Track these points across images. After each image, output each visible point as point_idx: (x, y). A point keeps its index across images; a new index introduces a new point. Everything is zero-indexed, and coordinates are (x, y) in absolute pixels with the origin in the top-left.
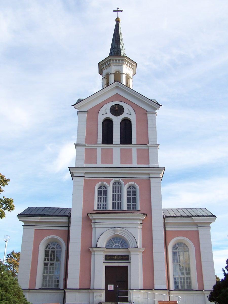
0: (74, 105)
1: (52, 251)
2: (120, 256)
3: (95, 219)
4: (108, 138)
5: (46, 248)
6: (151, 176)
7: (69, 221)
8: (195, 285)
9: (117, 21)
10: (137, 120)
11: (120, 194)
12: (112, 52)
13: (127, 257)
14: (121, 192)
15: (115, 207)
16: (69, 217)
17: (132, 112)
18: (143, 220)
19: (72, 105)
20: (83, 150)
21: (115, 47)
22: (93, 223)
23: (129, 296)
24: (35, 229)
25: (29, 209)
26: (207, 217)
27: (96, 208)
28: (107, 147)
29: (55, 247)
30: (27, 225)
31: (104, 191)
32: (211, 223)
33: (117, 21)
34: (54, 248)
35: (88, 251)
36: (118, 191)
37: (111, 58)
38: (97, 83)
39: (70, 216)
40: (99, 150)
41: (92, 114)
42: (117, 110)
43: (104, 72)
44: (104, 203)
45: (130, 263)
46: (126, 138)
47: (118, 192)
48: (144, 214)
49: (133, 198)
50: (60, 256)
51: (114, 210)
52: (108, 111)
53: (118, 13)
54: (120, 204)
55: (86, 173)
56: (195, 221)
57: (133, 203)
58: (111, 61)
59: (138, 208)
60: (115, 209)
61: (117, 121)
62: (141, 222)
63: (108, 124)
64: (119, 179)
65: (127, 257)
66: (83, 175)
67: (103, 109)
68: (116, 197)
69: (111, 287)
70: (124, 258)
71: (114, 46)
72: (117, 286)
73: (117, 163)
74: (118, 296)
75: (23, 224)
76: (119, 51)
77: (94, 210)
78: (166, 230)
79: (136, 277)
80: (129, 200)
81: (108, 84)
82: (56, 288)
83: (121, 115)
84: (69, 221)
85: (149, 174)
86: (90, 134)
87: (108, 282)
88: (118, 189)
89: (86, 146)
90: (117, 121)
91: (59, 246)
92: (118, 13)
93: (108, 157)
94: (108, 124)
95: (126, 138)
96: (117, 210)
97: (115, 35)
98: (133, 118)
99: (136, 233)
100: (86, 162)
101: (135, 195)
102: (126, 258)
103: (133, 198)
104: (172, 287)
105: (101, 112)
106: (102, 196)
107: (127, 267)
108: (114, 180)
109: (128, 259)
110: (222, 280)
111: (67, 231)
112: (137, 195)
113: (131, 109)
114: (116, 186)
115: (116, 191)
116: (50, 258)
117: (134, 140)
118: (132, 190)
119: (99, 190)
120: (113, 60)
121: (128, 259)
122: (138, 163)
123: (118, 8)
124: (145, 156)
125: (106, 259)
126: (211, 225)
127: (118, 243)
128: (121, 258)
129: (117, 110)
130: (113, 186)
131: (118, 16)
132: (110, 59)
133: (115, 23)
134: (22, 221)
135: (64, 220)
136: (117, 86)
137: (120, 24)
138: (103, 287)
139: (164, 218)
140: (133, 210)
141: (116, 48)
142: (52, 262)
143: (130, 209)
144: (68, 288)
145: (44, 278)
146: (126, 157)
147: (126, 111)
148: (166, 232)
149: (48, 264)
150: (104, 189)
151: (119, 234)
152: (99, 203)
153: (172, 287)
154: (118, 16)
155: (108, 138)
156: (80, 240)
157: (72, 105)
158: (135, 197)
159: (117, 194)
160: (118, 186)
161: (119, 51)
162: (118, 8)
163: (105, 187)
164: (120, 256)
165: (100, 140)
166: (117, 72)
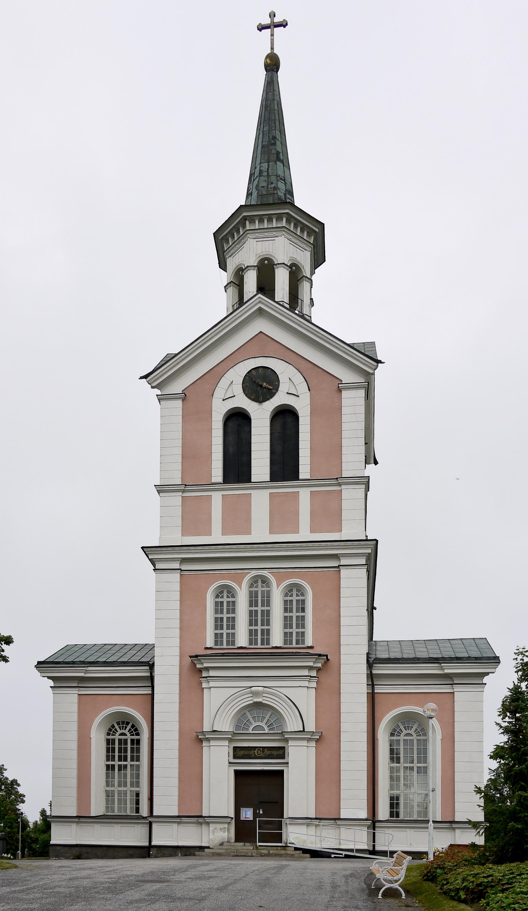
0: (145, 377)
1: (120, 740)
2: (267, 749)
3: (207, 669)
4: (237, 468)
5: (392, 734)
6: (343, 562)
7: (151, 674)
8: (436, 812)
9: (272, 65)
10: (313, 412)
11: (268, 608)
12: (254, 190)
13: (281, 752)
14: (268, 605)
15: (256, 640)
16: (151, 666)
17: (302, 388)
18: (319, 670)
19: (141, 378)
20: (176, 499)
21: (261, 172)
22: (206, 677)
23: (284, 831)
24: (79, 695)
25: (67, 648)
26: (478, 661)
27: (210, 642)
28: (237, 490)
29: (126, 732)
30: (59, 683)
31: (228, 602)
32: (487, 674)
33: (272, 65)
34: (125, 735)
35: (196, 740)
36: (263, 602)
37: (245, 214)
38: (207, 298)
39: (154, 663)
40: (217, 498)
41: (193, 402)
42: (260, 384)
43: (232, 263)
44: (230, 631)
45: (287, 763)
46: (285, 466)
47: (263, 605)
48: (320, 655)
49: (297, 617)
50: (138, 750)
51: (288, 646)
52: (238, 389)
53: (272, 35)
54: (267, 633)
55: (184, 561)
56: (447, 671)
57: (298, 630)
58: (247, 222)
59: (309, 642)
60: (256, 644)
61: (261, 416)
62: (314, 673)
63: (238, 421)
64: (265, 573)
65: (281, 752)
66: (176, 565)
67: (224, 382)
68: (256, 615)
69: (247, 814)
70: (275, 753)
71: (258, 169)
72: (259, 812)
73: (260, 531)
74: (258, 831)
75: (51, 683)
76: (272, 183)
77: (207, 648)
78: (376, 691)
79: (299, 794)
80: (287, 622)
81: (241, 301)
82: (135, 814)
83: (271, 398)
84: (151, 674)
85: (336, 557)
86: (192, 455)
87: (240, 803)
88: (263, 597)
89: (184, 491)
90: (261, 416)
91: (135, 730)
92: (272, 35)
93: (238, 517)
94: (238, 421)
95: (285, 466)
96: (259, 646)
97: (262, 125)
98: (303, 407)
99: (297, 700)
100: (185, 532)
101: (303, 610)
102: (280, 753)
103: (297, 617)
104: (383, 812)
105: (219, 393)
106: (225, 616)
107: (282, 772)
108: (254, 573)
109: (283, 757)
110: (36, 823)
111: (150, 697)
112: (306, 610)
113: (298, 378)
114: (256, 589)
115: (257, 601)
116: (117, 754)
117: (304, 471)
118: (294, 598)
119: (217, 600)
120: (252, 220)
121: (283, 757)
122: (313, 530)
123: (272, 15)
124: (328, 513)
125: (235, 757)
126: (486, 680)
127: (251, 724)
128: (269, 752)
129: (260, 384)
130: (251, 589)
131: (272, 48)
132: (245, 218)
133: (260, 76)
134: (49, 678)
135: (143, 672)
136: (260, 309)
137: (283, 76)
138: (232, 815)
139: (370, 665)
140: (298, 646)
141: (265, 174)
142: (123, 763)
143: (291, 643)
144: (154, 814)
145: (109, 795)
146: (283, 515)
147: (284, 387)
148: (376, 695)
149: (113, 766)
150: (228, 597)
151: (264, 702)
152: (217, 632)
153: (383, 812)
154: (272, 48)
155: (237, 468)
156: (175, 717)
157: (141, 378)
158: (303, 614)
159: (259, 608)
160: (263, 589)
161: (273, 186)
162: (272, 15)
163: (231, 592)
164: (266, 750)
165: (217, 474)
166: (266, 262)
